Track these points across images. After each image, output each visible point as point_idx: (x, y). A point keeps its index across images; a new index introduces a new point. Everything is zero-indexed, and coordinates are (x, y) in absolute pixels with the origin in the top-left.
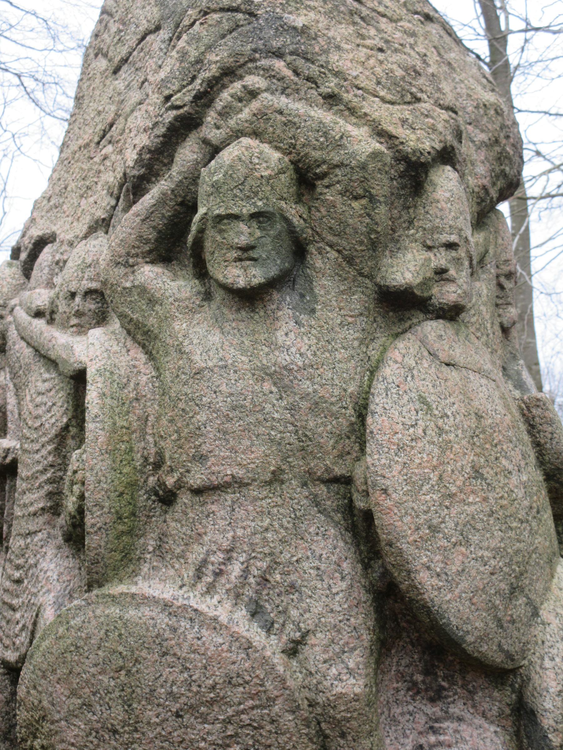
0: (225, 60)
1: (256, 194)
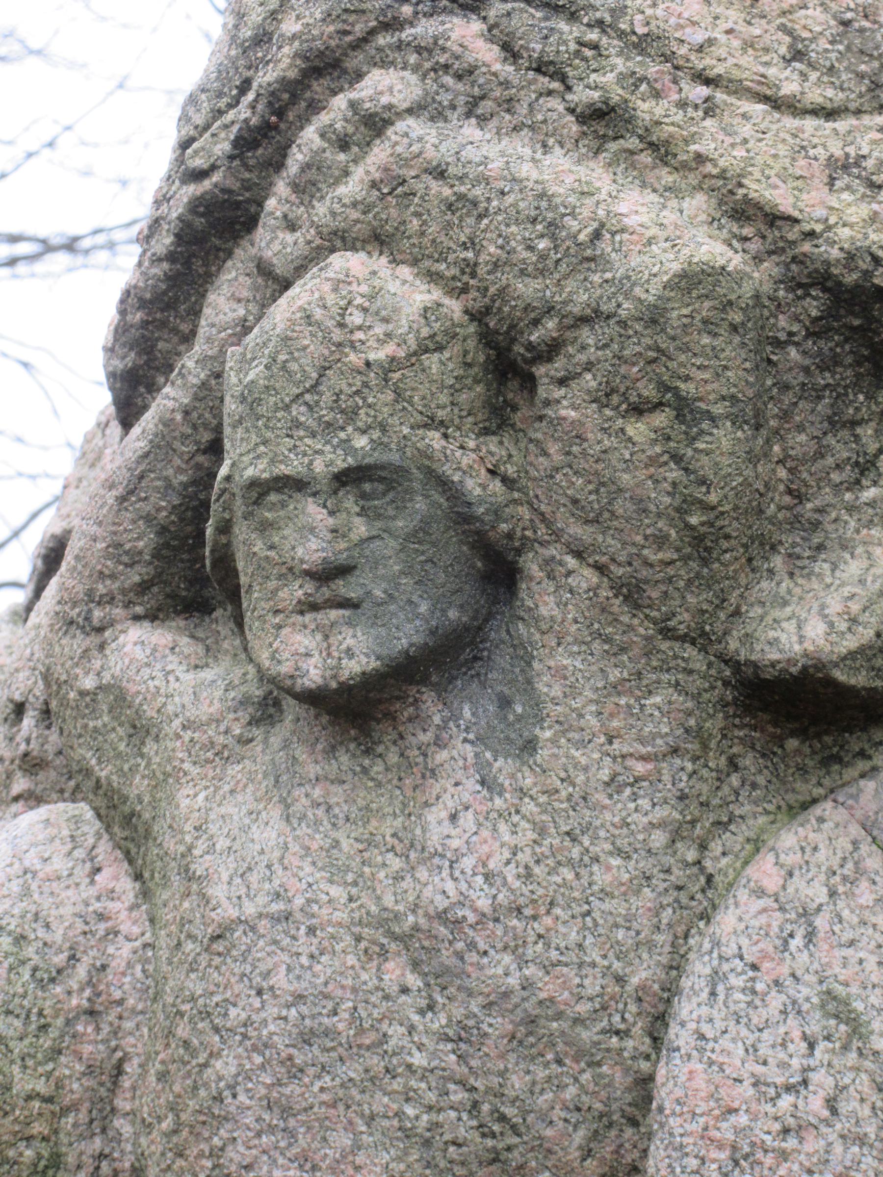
0: (315, 32)
1: (351, 414)
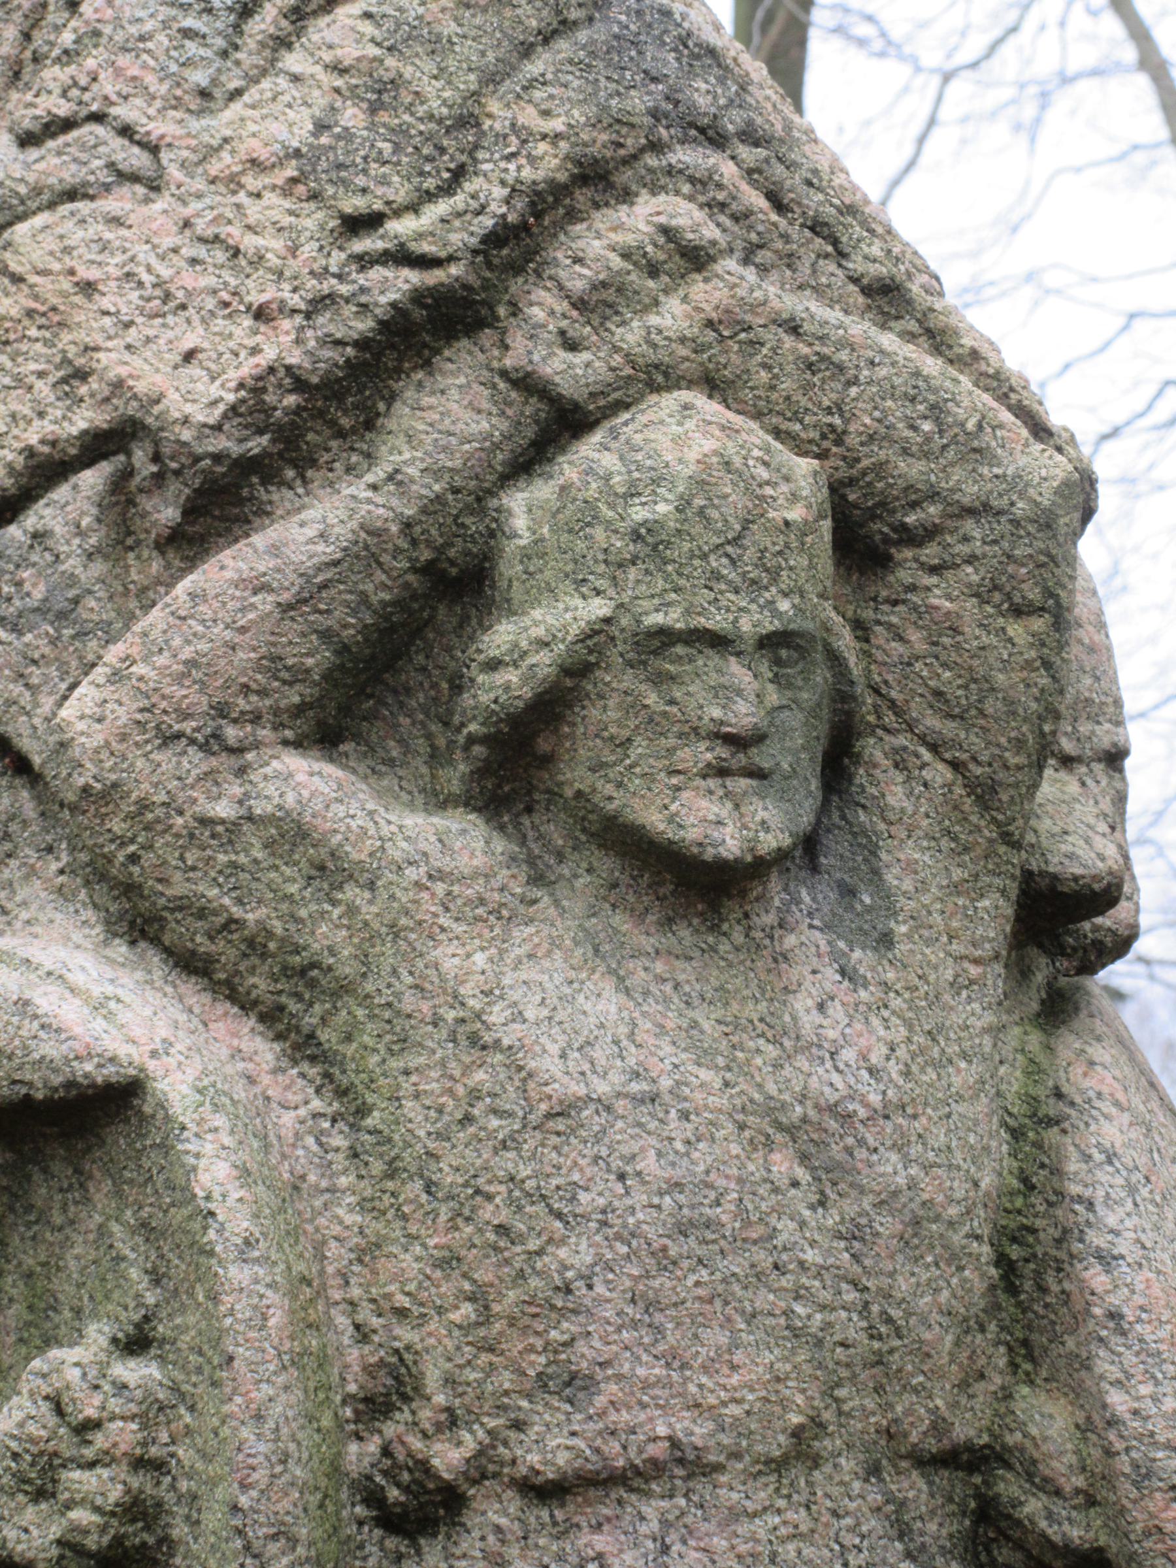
0: (585, 136)
1: (774, 575)
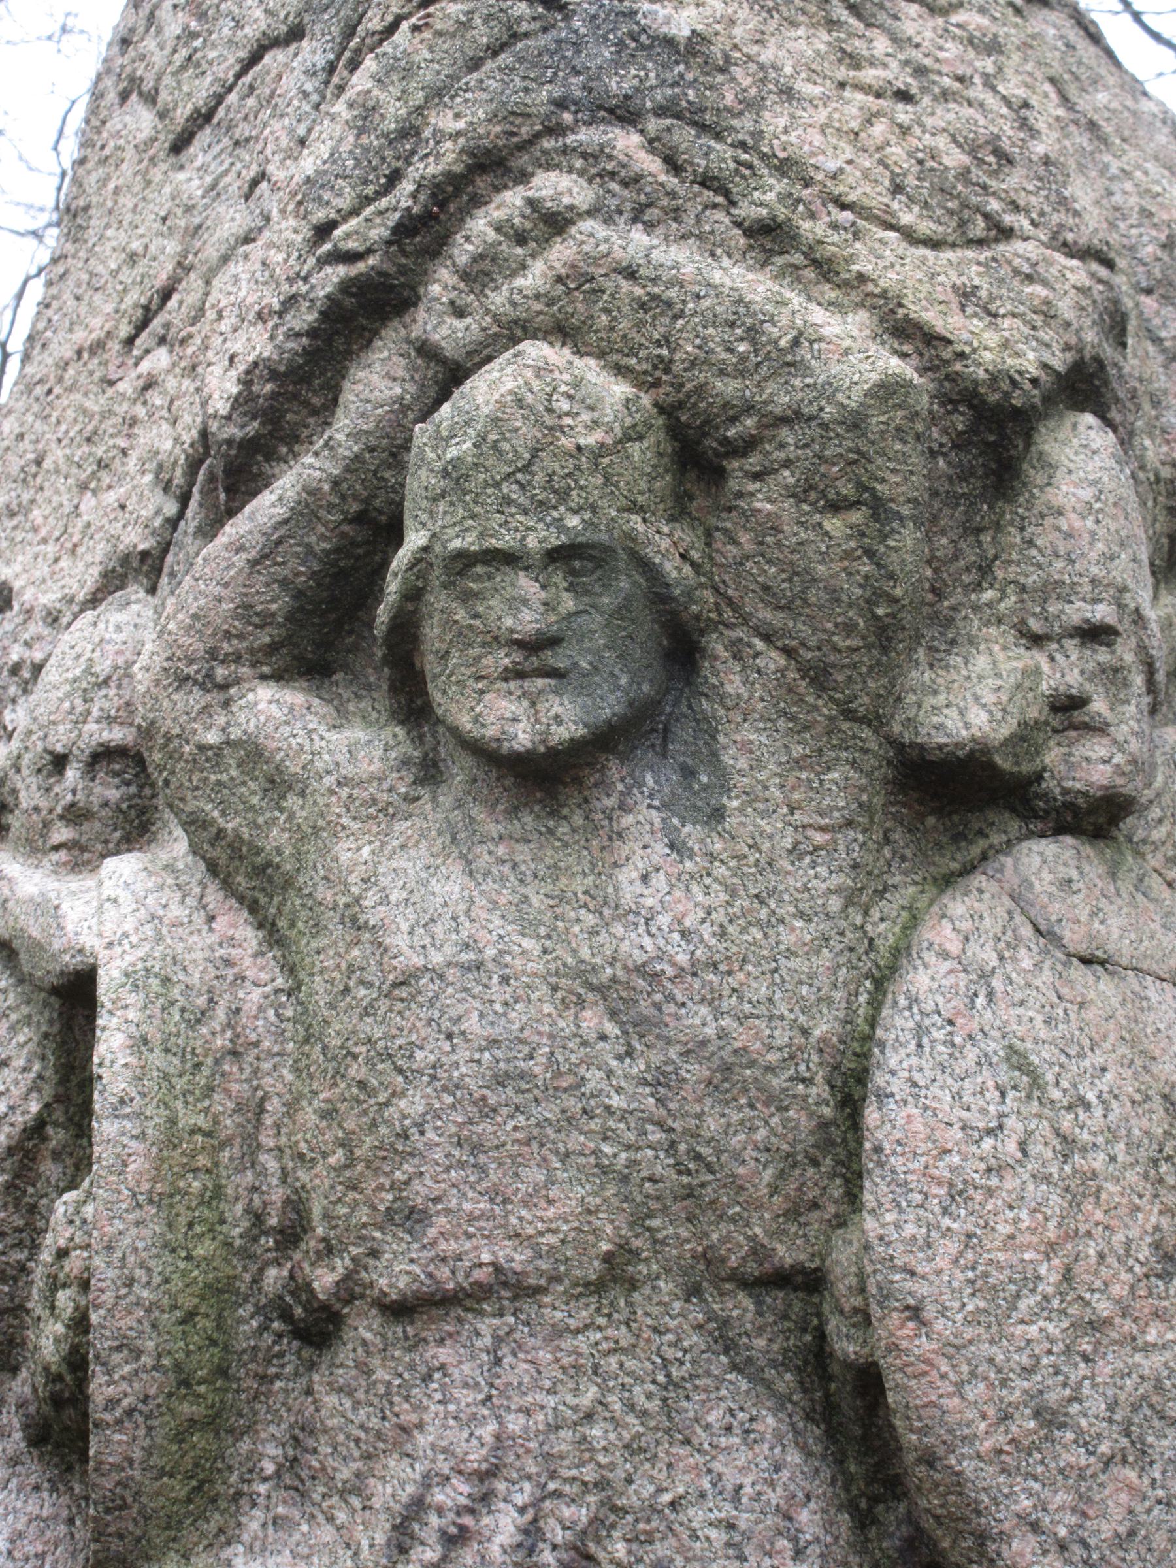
0: (481, 131)
1: (563, 495)
